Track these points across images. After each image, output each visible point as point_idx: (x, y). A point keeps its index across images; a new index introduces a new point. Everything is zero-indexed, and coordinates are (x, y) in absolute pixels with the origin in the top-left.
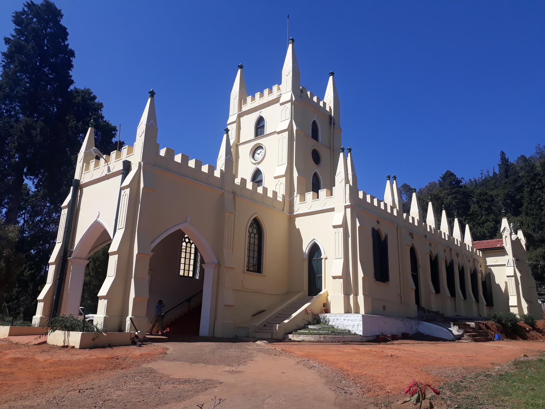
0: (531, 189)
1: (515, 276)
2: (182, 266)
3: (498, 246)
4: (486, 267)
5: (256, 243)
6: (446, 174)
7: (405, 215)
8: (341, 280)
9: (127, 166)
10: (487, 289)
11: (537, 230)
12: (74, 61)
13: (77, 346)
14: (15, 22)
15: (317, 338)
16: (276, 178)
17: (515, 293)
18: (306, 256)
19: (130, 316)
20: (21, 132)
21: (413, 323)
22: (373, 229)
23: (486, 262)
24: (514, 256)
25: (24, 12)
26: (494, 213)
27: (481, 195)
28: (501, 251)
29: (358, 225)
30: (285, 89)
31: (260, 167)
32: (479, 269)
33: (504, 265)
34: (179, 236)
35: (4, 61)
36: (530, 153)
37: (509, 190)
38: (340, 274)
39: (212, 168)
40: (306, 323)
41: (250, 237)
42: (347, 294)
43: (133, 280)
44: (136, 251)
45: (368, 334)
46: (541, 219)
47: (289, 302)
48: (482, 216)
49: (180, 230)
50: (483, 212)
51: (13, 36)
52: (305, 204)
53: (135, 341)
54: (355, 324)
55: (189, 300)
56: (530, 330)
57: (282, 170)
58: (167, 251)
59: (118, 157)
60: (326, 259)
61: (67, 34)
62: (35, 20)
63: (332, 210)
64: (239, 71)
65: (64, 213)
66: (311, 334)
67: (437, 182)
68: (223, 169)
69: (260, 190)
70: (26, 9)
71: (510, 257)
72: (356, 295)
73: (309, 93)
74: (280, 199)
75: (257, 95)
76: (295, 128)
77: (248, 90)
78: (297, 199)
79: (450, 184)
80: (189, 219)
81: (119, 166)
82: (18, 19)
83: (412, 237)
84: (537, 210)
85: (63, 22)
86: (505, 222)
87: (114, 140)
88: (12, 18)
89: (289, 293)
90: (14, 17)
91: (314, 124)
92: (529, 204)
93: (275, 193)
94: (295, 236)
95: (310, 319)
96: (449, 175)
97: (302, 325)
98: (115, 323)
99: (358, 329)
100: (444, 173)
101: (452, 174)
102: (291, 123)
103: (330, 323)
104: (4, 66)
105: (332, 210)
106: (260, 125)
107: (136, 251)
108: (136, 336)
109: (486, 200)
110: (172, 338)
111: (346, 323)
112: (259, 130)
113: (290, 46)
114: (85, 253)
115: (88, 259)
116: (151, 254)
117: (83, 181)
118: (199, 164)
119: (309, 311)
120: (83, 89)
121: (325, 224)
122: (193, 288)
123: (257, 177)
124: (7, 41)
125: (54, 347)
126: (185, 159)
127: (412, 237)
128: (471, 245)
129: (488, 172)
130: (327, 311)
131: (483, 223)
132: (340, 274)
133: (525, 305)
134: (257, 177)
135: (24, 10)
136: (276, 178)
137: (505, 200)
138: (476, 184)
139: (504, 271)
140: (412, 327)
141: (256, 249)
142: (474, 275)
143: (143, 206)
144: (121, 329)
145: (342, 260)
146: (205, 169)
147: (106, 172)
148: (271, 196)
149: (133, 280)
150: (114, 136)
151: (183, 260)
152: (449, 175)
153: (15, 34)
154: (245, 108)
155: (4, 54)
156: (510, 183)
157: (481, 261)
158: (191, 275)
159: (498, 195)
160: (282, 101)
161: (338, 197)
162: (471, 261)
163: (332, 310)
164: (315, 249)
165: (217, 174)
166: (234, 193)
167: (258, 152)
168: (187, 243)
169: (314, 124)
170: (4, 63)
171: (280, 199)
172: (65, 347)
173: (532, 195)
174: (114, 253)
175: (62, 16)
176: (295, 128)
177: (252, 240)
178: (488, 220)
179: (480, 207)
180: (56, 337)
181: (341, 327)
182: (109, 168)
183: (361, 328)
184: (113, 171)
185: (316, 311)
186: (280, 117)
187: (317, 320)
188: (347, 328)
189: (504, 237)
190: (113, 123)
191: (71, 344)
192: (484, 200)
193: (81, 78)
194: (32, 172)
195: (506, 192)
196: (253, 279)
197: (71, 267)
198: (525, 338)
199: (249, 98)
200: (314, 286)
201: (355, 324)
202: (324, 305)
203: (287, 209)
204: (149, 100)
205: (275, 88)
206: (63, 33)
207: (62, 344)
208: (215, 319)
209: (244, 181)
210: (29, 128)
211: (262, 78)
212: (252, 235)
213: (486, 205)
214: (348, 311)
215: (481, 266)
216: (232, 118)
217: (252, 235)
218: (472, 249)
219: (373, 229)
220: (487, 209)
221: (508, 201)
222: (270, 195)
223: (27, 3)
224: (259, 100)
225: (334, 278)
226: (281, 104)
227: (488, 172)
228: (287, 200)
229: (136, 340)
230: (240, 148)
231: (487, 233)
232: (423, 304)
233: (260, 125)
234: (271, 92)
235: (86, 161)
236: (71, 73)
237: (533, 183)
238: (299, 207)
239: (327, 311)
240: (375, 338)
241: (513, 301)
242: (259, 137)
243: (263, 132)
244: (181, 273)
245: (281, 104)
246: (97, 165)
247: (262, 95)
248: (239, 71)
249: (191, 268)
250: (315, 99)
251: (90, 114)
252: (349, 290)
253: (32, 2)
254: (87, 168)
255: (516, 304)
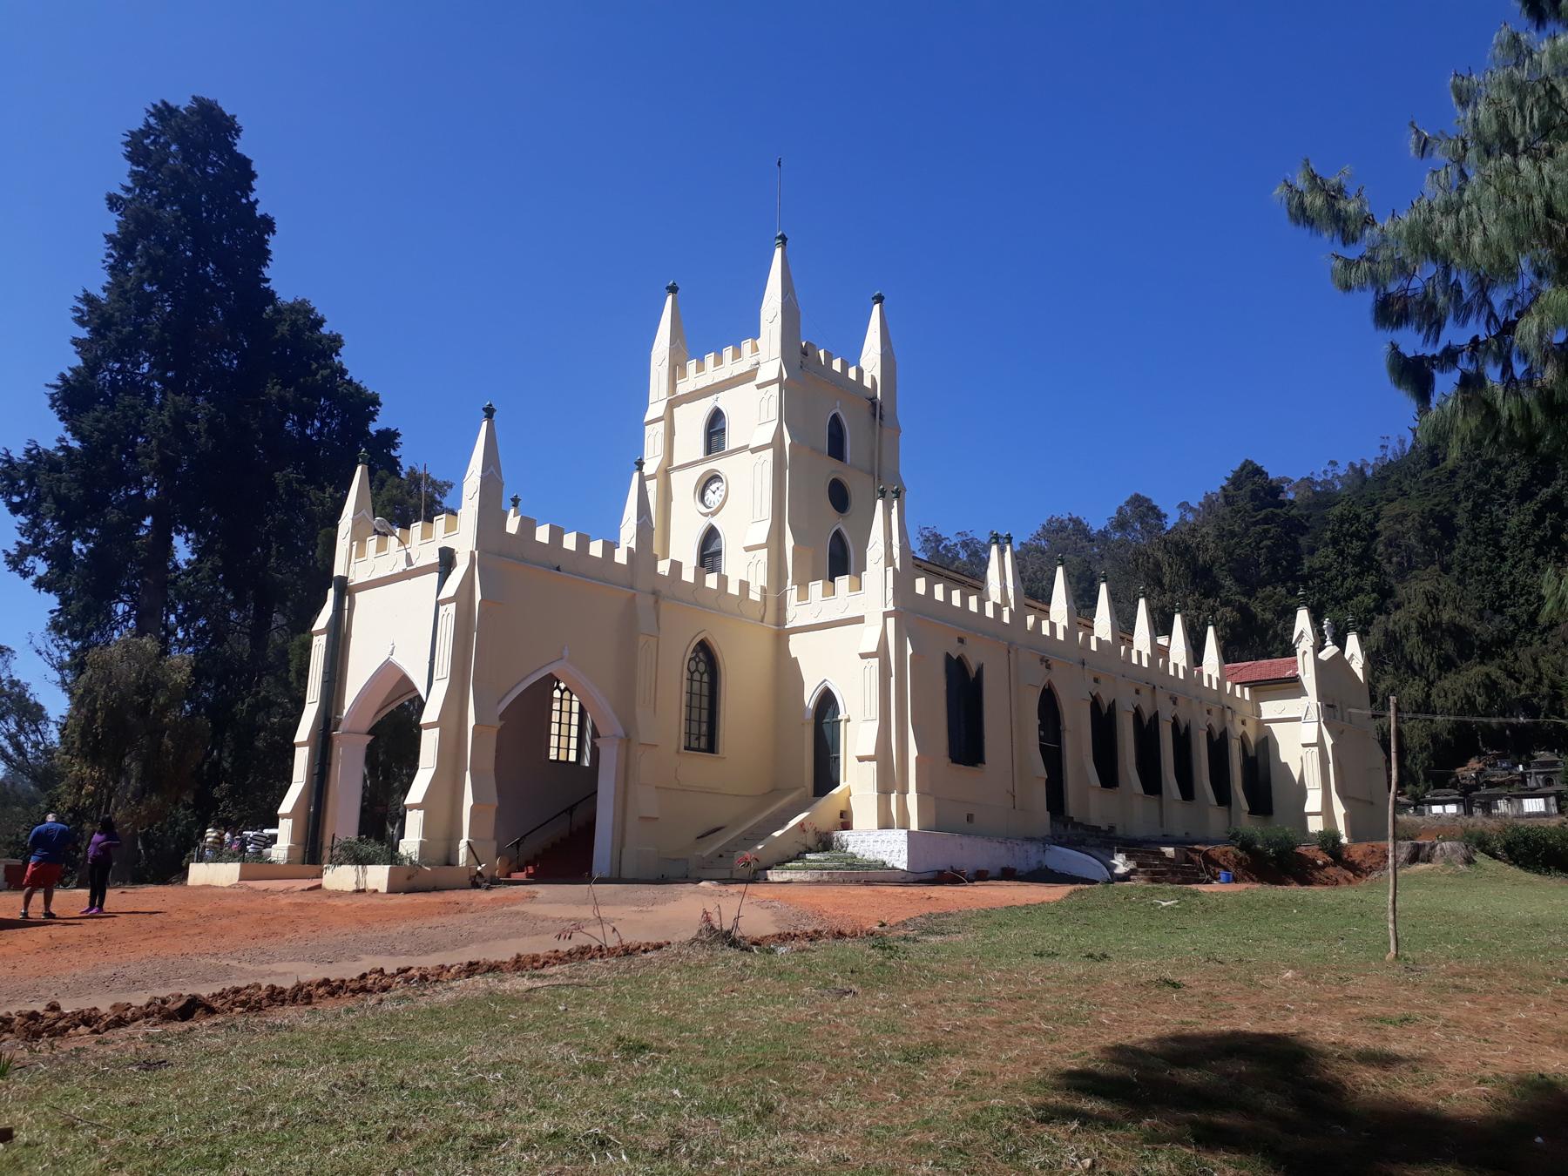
0: (1475, 504)
1: (1320, 743)
2: (554, 741)
3: (1288, 674)
4: (1260, 724)
5: (705, 691)
6: (1243, 468)
7: (1031, 620)
8: (874, 764)
9: (447, 560)
10: (1261, 775)
11: (1488, 613)
12: (273, 243)
13: (383, 888)
14: (130, 157)
15: (816, 875)
16: (748, 549)
17: (1318, 784)
18: (810, 716)
19: (466, 838)
20: (166, 429)
21: (1032, 849)
22: (948, 656)
23: (1259, 714)
24: (1321, 696)
25: (147, 131)
26: (1378, 570)
27: (1342, 520)
28: (1291, 686)
29: (910, 651)
30: (766, 352)
31: (716, 522)
32: (1237, 729)
33: (1298, 719)
34: (550, 682)
35: (110, 256)
36: (1319, 471)
37: (1436, 501)
38: (872, 752)
39: (610, 547)
40: (802, 849)
41: (691, 680)
42: (884, 791)
43: (468, 773)
44: (471, 722)
45: (922, 868)
46: (1499, 583)
47: (773, 809)
48: (1344, 579)
49: (551, 675)
50: (1349, 568)
51: (128, 190)
52: (809, 605)
53: (476, 882)
54: (893, 849)
55: (570, 810)
56: (1326, 864)
57: (761, 533)
58: (524, 719)
59: (426, 535)
60: (848, 720)
61: (253, 176)
62: (173, 148)
63: (859, 620)
64: (670, 299)
65: (319, 645)
66: (806, 869)
67: (1218, 490)
68: (633, 545)
69: (711, 581)
70: (152, 121)
71: (1310, 702)
72: (904, 792)
73: (822, 353)
74: (755, 596)
75: (710, 359)
76: (788, 440)
77: (689, 347)
78: (792, 594)
79: (1254, 495)
80: (566, 653)
81: (428, 555)
82: (137, 149)
83: (1048, 667)
84: (1491, 560)
85: (241, 147)
86: (1303, 619)
87: (373, 428)
88: (123, 149)
89: (775, 792)
90: (127, 144)
91: (836, 423)
92: (1469, 543)
93: (744, 586)
94: (786, 672)
95: (810, 840)
96: (1251, 472)
97: (793, 853)
98: (439, 851)
99: (900, 861)
100: (1237, 467)
101: (1258, 471)
102: (779, 430)
103: (850, 849)
104: (112, 267)
105: (859, 620)
106: (715, 427)
107: (471, 722)
108: (479, 873)
109: (1356, 535)
110: (540, 878)
111: (878, 847)
112: (715, 438)
113: (778, 252)
114: (367, 722)
115: (369, 733)
116: (499, 724)
117: (356, 578)
118: (583, 542)
119: (807, 826)
120: (291, 301)
121: (845, 646)
122: (578, 784)
123: (709, 550)
124: (113, 202)
125: (339, 894)
126: (557, 534)
127: (1048, 667)
128: (1216, 675)
129: (1402, 442)
130: (847, 826)
131: (1349, 597)
132: (872, 752)
133: (1339, 810)
134: (709, 550)
135: (148, 125)
136: (748, 549)
137: (1424, 527)
138: (1322, 498)
139: (1297, 733)
140: (1030, 856)
141: (705, 704)
142: (1218, 747)
143: (481, 634)
144: (450, 860)
145: (877, 724)
146: (596, 549)
147: (401, 566)
148: (736, 593)
149: (468, 773)
150: (371, 417)
151: (555, 729)
152: (1251, 472)
153: (128, 183)
154: (683, 388)
155: (110, 238)
156: (1440, 483)
157: (1248, 710)
158: (572, 758)
159: (1405, 516)
160: (760, 379)
161: (871, 594)
162: (1215, 711)
163: (855, 824)
164: (827, 701)
165: (621, 557)
166: (655, 593)
167: (713, 487)
168: (562, 692)
169: (836, 423)
170: (111, 260)
171: (755, 596)
172: (358, 891)
173: (1478, 519)
174: (430, 726)
175: (238, 131)
176: (788, 440)
177: (696, 685)
178: (1362, 590)
179: (1341, 553)
180: (340, 877)
181: (869, 856)
182: (408, 555)
183: (905, 857)
184: (418, 564)
185: (823, 828)
186: (756, 416)
187: (825, 843)
188: (880, 857)
189: (1299, 652)
190: (370, 387)
191: (371, 886)
192: (1352, 535)
193: (287, 277)
194: (193, 524)
195: (1427, 505)
196: (700, 768)
197: (339, 751)
198: (1305, 880)
199: (692, 365)
200: (825, 776)
201: (893, 849)
202: (842, 814)
203: (770, 615)
204: (485, 424)
205: (747, 346)
206: (243, 172)
207: (354, 887)
208: (622, 845)
209: (676, 567)
210: (181, 419)
211: (716, 326)
212: (697, 676)
213: (1356, 547)
214: (885, 824)
215: (1243, 723)
216: (655, 409)
217: (697, 676)
218: (1221, 683)
219: (948, 656)
220: (1358, 561)
221: (1433, 531)
222: (733, 589)
223: (155, 106)
224: (712, 373)
225: (861, 759)
226: (759, 387)
227: (1402, 442)
228: (772, 595)
229: (478, 880)
230: (674, 476)
231: (1256, 640)
232: (1072, 807)
233: (715, 427)
234: (737, 355)
235: (358, 536)
236: (266, 272)
237: (1482, 486)
238: (797, 614)
239: (847, 826)
240: (930, 873)
241: (1313, 802)
242: (709, 464)
243: (721, 446)
244: (553, 755)
245: (759, 387)
246: (381, 548)
247: (719, 361)
248: (670, 299)
249: (574, 743)
250: (837, 365)
251: (314, 366)
252: (888, 783)
253: (164, 103)
254: (361, 553)
255: (1321, 808)
